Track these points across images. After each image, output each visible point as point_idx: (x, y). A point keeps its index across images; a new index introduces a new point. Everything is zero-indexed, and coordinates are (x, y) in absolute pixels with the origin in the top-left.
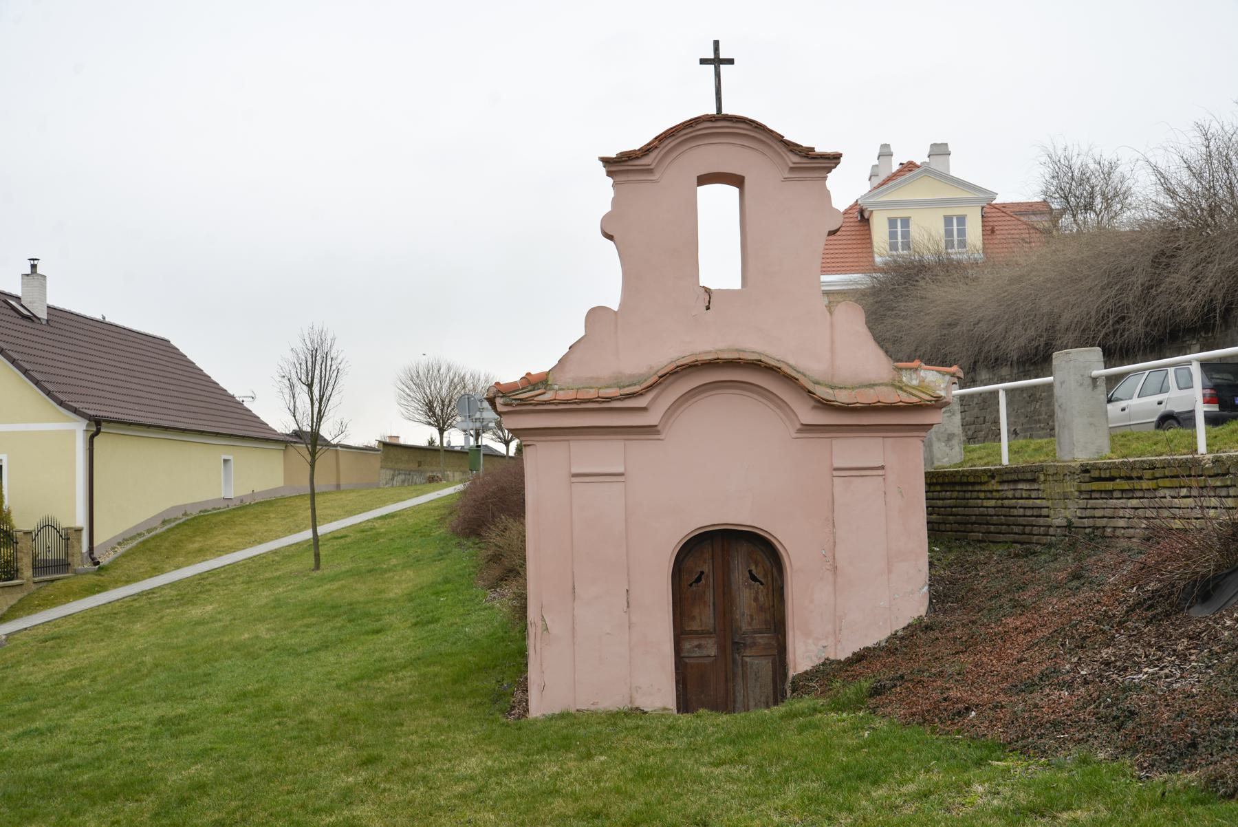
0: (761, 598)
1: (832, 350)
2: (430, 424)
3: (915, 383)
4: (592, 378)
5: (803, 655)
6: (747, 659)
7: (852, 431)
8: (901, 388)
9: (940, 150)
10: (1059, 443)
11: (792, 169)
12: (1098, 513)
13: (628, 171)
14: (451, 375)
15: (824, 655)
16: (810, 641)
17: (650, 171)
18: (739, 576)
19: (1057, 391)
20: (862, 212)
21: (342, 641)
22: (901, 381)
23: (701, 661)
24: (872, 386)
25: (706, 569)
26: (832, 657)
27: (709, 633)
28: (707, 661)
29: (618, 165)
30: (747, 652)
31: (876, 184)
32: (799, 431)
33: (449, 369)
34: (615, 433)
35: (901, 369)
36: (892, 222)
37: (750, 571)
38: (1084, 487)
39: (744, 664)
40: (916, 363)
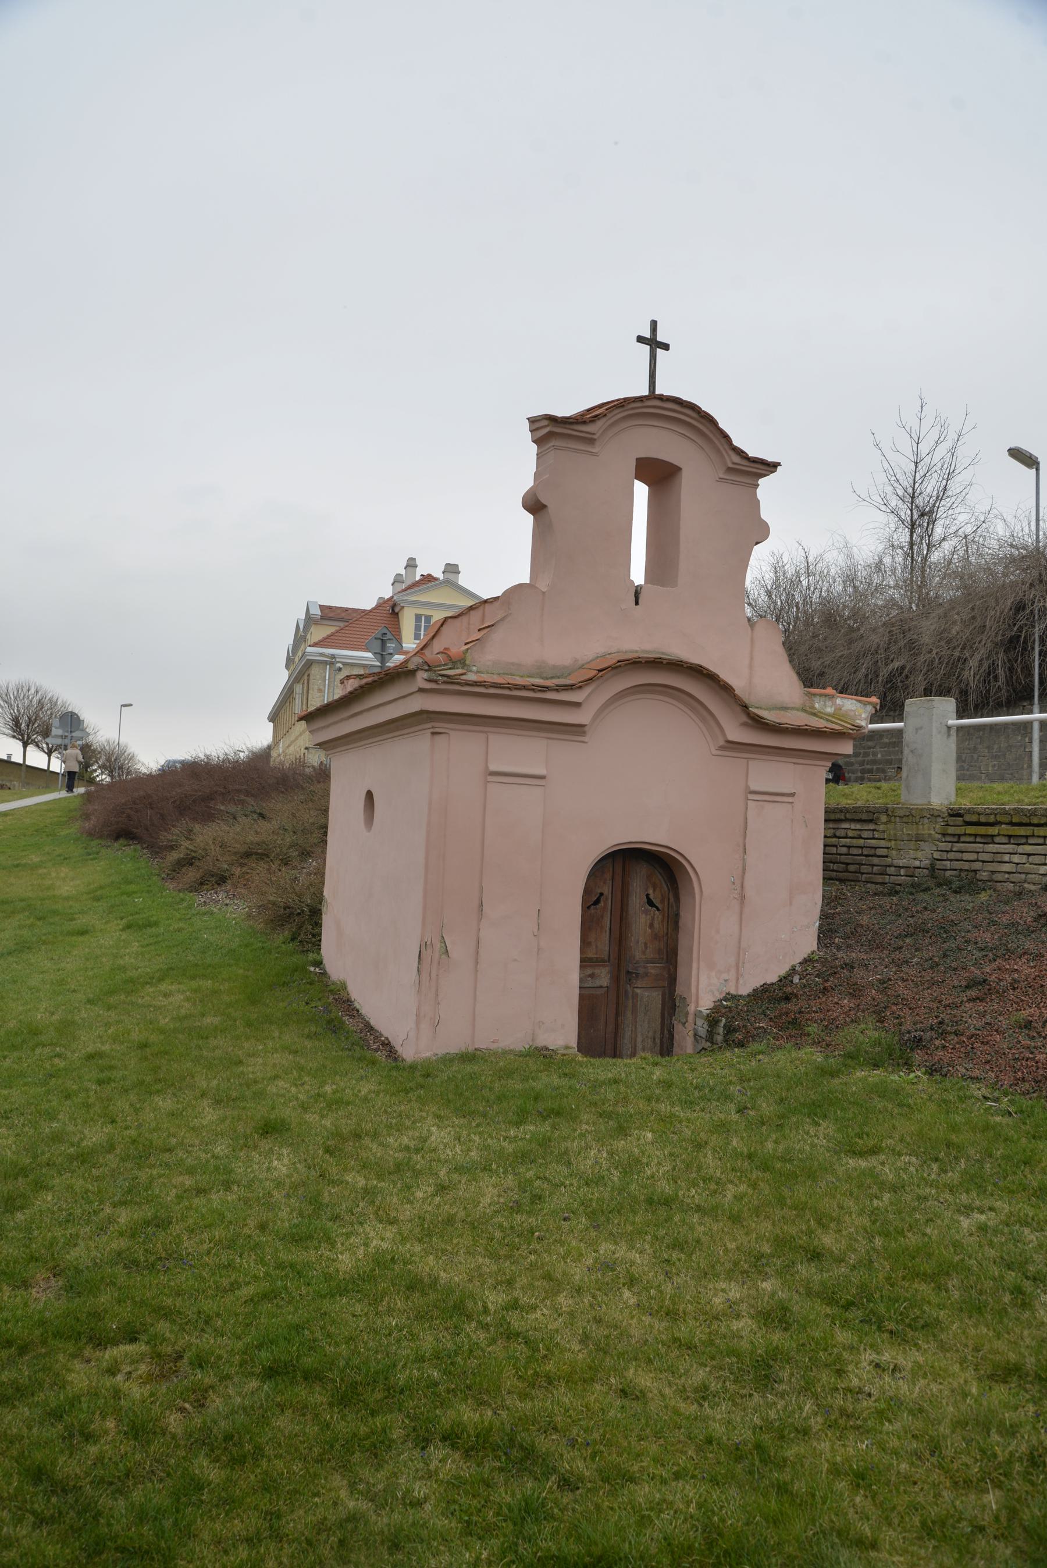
0: (656, 925)
1: (751, 667)
2: (14, 737)
3: (829, 710)
4: (513, 664)
5: (706, 986)
6: (638, 991)
7: (769, 754)
8: (815, 715)
9: (452, 569)
10: (908, 787)
11: (730, 470)
12: (966, 856)
13: (569, 436)
14: (39, 696)
15: (725, 990)
16: (713, 974)
17: (591, 441)
18: (637, 900)
19: (907, 737)
20: (394, 606)
21: (44, 943)
22: (813, 707)
23: (593, 992)
24: (785, 709)
25: (606, 890)
26: (733, 992)
27: (603, 961)
28: (599, 992)
29: (550, 431)
30: (639, 984)
31: (399, 589)
32: (722, 748)
33: (37, 692)
34: (539, 730)
35: (815, 695)
36: (418, 617)
37: (648, 895)
38: (951, 830)
39: (635, 996)
40: (830, 691)
